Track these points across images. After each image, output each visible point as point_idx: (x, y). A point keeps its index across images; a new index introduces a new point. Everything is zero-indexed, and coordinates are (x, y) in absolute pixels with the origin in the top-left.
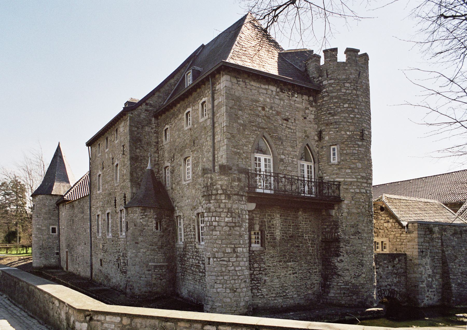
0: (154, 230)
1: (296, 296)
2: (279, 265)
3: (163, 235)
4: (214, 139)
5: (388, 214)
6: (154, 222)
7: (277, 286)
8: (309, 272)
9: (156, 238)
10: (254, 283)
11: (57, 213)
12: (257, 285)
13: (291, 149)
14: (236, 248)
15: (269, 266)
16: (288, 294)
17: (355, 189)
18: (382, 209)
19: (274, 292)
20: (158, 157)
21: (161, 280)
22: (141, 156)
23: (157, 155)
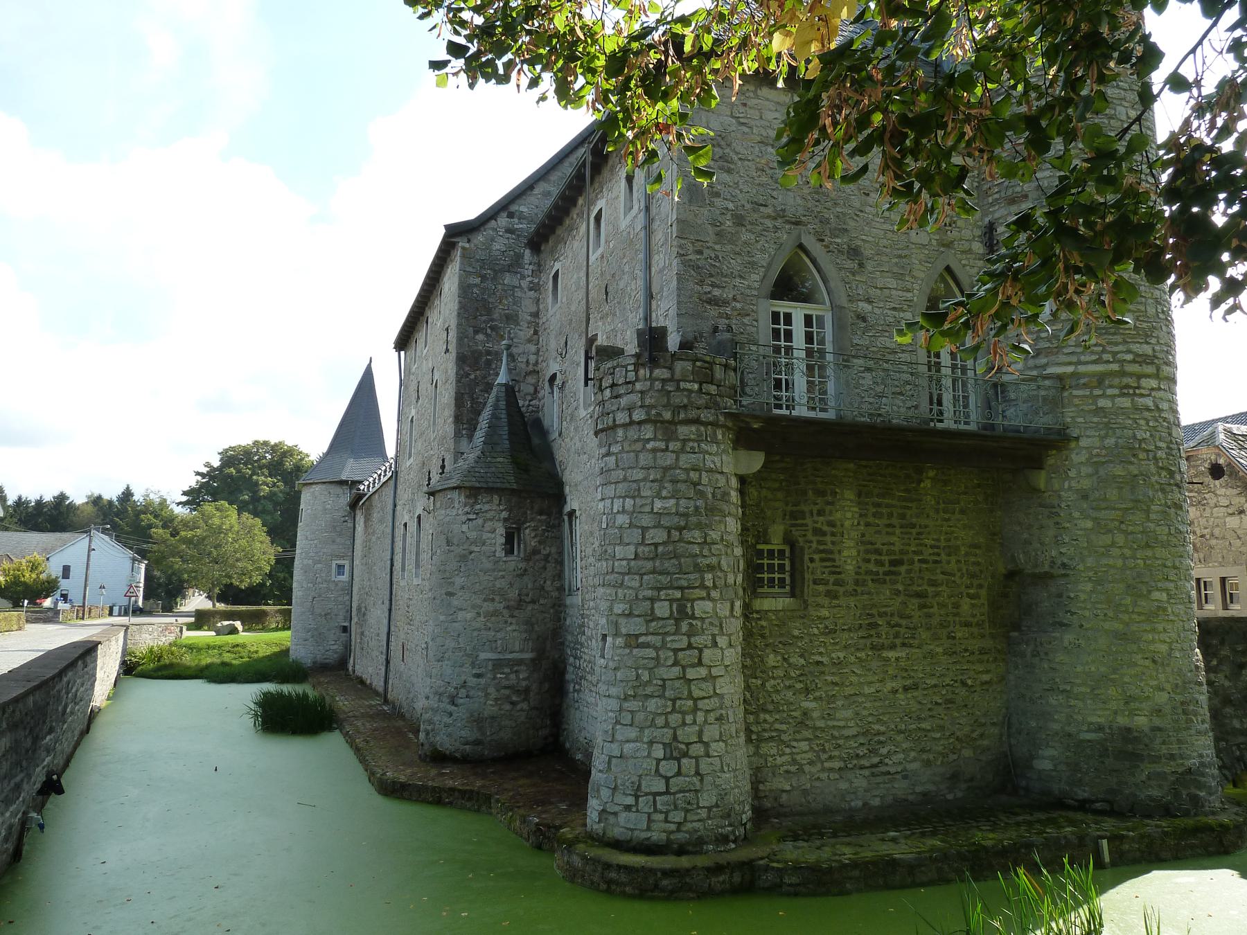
0: (500, 553)
3: (526, 570)
4: (648, 267)
5: (1238, 487)
6: (501, 531)
7: (847, 732)
8: (964, 684)
9: (503, 577)
10: (765, 721)
11: (350, 528)
12: (777, 726)
13: (892, 283)
15: (818, 663)
16: (887, 761)
17: (1113, 397)
18: (1216, 471)
19: (836, 753)
21: (513, 703)
22: (488, 353)
23: (533, 348)
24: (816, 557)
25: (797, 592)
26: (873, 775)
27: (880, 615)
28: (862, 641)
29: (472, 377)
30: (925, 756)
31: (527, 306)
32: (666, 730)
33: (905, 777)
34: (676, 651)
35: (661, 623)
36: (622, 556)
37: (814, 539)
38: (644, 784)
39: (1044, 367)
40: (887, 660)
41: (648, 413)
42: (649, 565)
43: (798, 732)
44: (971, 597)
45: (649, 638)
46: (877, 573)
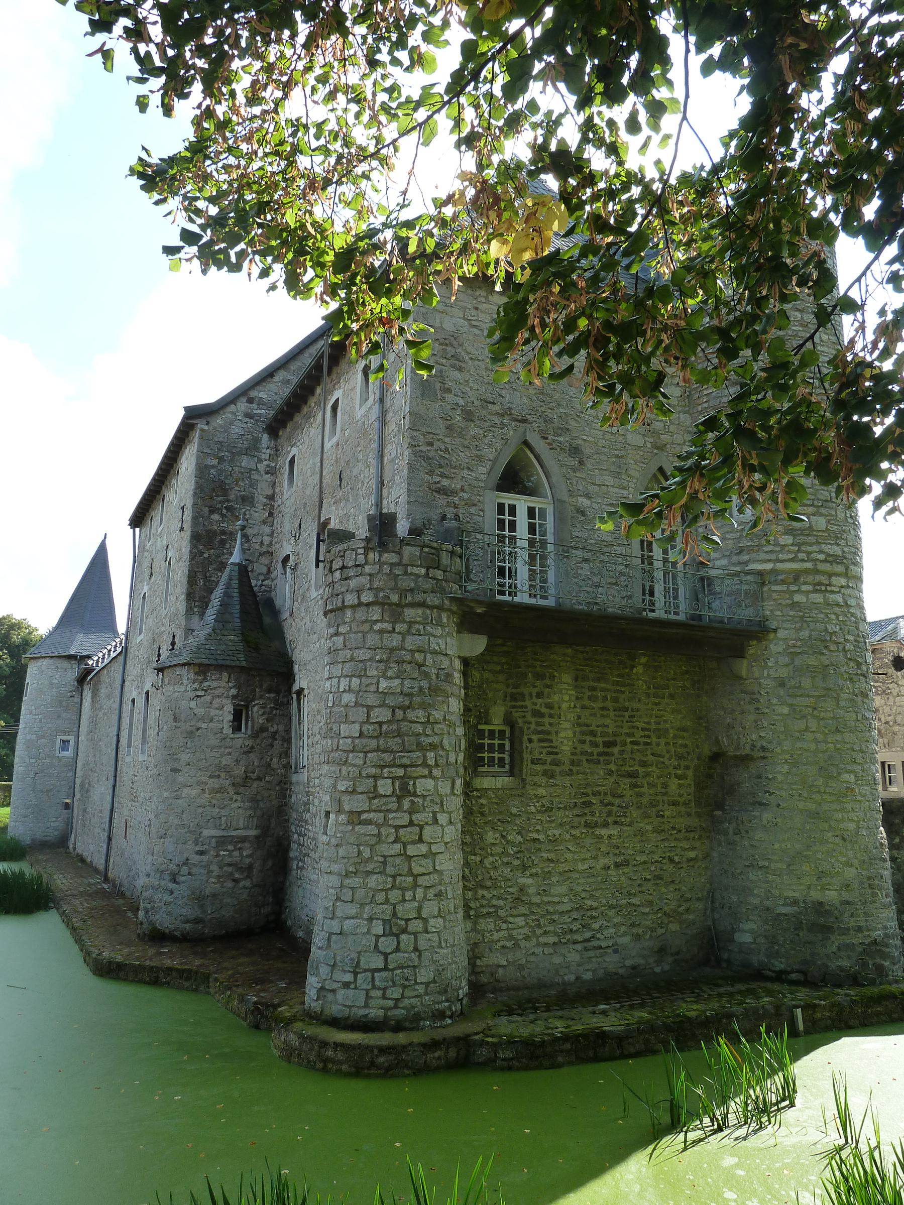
0: (228, 730)
1: (626, 940)
2: (568, 836)
3: (252, 747)
6: (229, 708)
8: (671, 860)
9: (230, 754)
10: (483, 897)
11: (77, 703)
12: (494, 902)
13: (610, 480)
14: (410, 778)
16: (599, 935)
20: (271, 535)
21: (236, 881)
22: (223, 533)
23: (267, 530)
24: (535, 737)
25: (516, 771)
26: (586, 949)
27: (594, 794)
28: (577, 819)
29: (206, 555)
30: (635, 931)
31: (263, 489)
32: (385, 906)
33: (616, 951)
34: (397, 828)
35: (384, 800)
36: (347, 734)
37: (533, 720)
38: (362, 959)
39: (746, 563)
40: (600, 837)
41: (376, 596)
42: (373, 743)
43: (515, 908)
44: (677, 777)
45: (372, 815)
46: (592, 754)
